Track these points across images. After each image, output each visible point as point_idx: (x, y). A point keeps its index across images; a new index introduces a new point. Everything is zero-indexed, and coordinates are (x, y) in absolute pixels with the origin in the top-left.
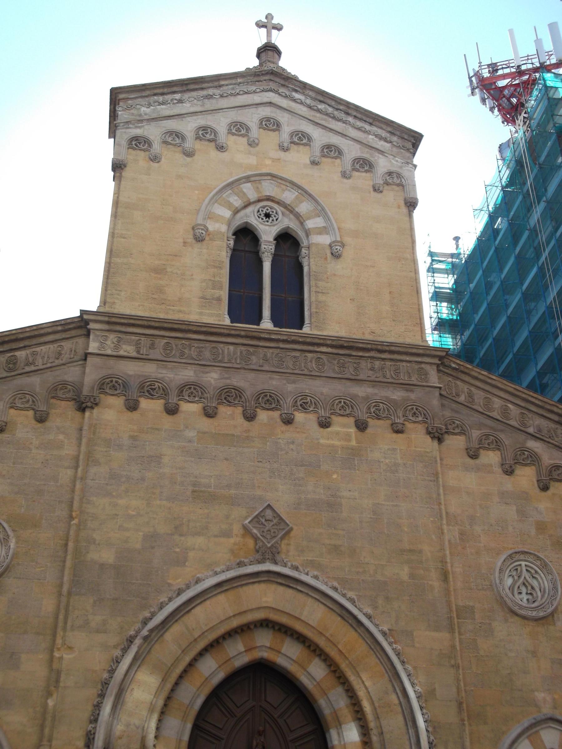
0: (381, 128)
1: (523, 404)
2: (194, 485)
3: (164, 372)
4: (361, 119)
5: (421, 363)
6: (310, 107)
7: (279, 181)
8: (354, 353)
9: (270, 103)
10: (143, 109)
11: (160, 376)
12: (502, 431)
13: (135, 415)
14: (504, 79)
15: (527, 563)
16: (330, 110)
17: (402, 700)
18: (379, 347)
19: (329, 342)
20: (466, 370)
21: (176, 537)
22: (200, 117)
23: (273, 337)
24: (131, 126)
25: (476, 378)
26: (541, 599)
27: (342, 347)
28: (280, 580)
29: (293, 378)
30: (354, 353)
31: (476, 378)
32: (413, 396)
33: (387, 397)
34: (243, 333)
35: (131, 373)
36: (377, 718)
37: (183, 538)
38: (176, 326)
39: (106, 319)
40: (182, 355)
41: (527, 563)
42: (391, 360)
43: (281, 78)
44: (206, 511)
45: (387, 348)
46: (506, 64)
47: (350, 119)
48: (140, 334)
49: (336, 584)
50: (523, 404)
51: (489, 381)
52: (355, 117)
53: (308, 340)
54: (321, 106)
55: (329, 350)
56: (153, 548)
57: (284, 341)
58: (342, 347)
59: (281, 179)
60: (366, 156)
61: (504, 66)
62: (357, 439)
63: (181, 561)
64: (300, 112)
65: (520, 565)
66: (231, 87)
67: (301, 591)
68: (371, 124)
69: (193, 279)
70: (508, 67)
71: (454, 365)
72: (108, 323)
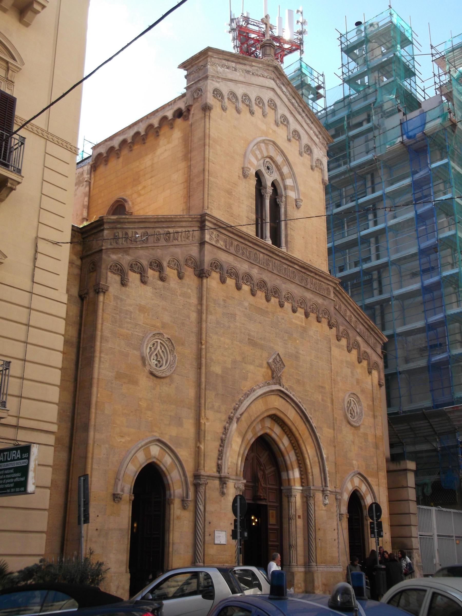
0: (316, 128)
1: (357, 316)
2: (249, 335)
3: (236, 263)
4: (308, 118)
5: (328, 284)
6: (289, 100)
7: (276, 147)
8: (307, 273)
9: (273, 89)
10: (219, 68)
11: (235, 265)
12: (349, 329)
13: (224, 286)
14: (254, 34)
15: (162, 342)
16: (296, 105)
17: (320, 460)
18: (317, 272)
19: (300, 264)
20: (341, 293)
21: (243, 364)
22: (244, 86)
23: (280, 254)
24: (214, 79)
25: (343, 298)
26: (166, 364)
27: (303, 268)
28: (281, 395)
29: (285, 280)
30: (307, 273)
31: (343, 298)
32: (325, 303)
33: (317, 301)
34: (269, 248)
35: (223, 260)
36: (311, 468)
37: (246, 365)
38: (243, 236)
39: (215, 222)
40: (243, 254)
41: (162, 342)
42: (319, 280)
43: (278, 72)
44: (254, 351)
45: (320, 274)
46: (256, 23)
47: (304, 115)
48: (227, 235)
49: (301, 401)
50: (357, 316)
51: (349, 301)
52: (306, 115)
53: (293, 260)
54: (293, 101)
55: (297, 268)
56: (235, 368)
57: (284, 258)
58: (303, 268)
59: (277, 147)
60: (310, 144)
61: (255, 24)
62: (305, 322)
63: (245, 378)
64: (284, 101)
65: (157, 342)
66: (256, 68)
67: (288, 402)
68: (312, 123)
69: (243, 203)
70: (258, 26)
71: (337, 289)
72: (215, 224)
